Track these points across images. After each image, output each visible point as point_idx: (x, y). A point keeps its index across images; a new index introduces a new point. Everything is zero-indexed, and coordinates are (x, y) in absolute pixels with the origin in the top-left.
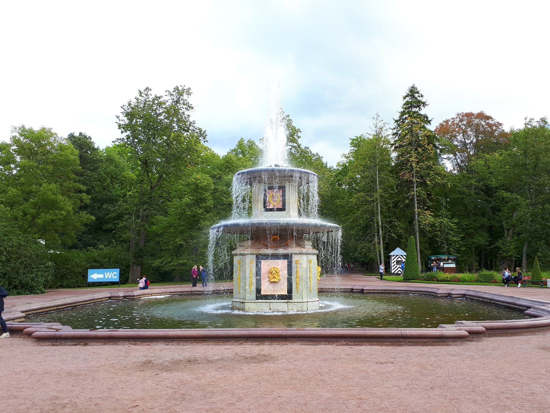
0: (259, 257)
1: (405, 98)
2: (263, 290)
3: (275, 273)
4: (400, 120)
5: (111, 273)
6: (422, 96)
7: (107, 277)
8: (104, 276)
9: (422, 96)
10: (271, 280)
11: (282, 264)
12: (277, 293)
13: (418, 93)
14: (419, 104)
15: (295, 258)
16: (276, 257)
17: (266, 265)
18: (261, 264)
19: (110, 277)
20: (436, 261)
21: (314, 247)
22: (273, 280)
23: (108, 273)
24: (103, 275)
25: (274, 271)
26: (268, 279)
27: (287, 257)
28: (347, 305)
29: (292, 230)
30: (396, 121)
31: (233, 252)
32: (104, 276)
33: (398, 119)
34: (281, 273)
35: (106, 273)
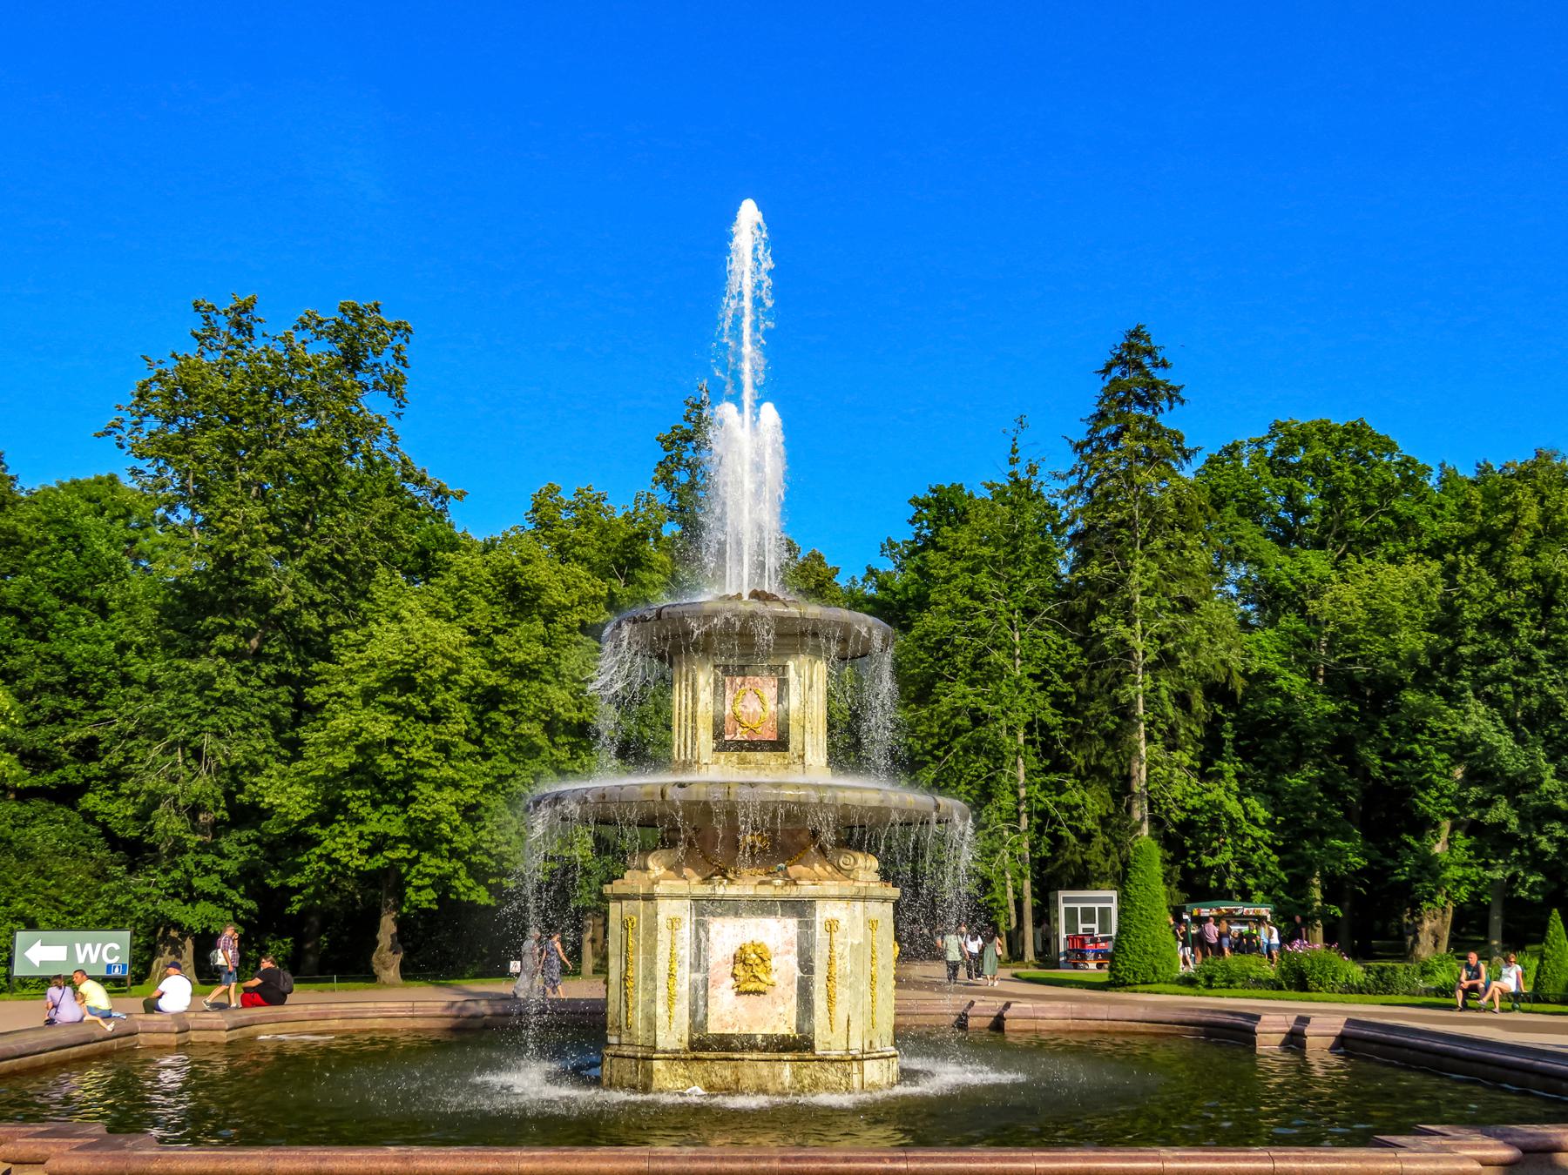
0: (705, 908)
1: (1108, 368)
2: (715, 1017)
3: (758, 961)
4: (1089, 443)
5: (99, 946)
6: (1164, 365)
7: (81, 959)
8: (71, 954)
9: (1164, 365)
10: (742, 988)
11: (777, 933)
12: (760, 1030)
13: (1149, 353)
14: (1151, 394)
15: (824, 912)
16: (762, 907)
17: (727, 935)
18: (707, 933)
19: (93, 959)
20: (1217, 920)
21: (885, 876)
22: (751, 986)
23: (88, 947)
24: (65, 948)
25: (754, 956)
26: (732, 982)
27: (800, 908)
28: (998, 1069)
29: (731, 813)
30: (1079, 447)
31: (607, 889)
32: (71, 954)
33: (1085, 438)
34: (773, 963)
35: (78, 946)
